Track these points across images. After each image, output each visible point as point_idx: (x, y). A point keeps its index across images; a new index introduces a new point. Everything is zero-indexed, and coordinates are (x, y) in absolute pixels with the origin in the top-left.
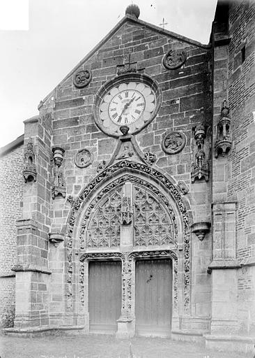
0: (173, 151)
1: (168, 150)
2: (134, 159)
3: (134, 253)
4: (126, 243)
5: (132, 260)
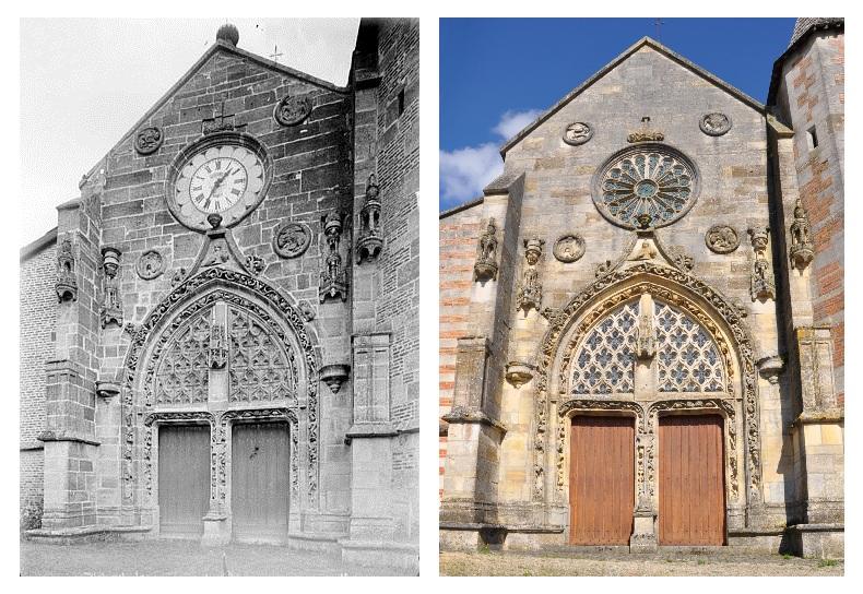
0: (723, 249)
1: (717, 245)
2: (660, 262)
3: (658, 403)
4: (647, 385)
5: (655, 414)
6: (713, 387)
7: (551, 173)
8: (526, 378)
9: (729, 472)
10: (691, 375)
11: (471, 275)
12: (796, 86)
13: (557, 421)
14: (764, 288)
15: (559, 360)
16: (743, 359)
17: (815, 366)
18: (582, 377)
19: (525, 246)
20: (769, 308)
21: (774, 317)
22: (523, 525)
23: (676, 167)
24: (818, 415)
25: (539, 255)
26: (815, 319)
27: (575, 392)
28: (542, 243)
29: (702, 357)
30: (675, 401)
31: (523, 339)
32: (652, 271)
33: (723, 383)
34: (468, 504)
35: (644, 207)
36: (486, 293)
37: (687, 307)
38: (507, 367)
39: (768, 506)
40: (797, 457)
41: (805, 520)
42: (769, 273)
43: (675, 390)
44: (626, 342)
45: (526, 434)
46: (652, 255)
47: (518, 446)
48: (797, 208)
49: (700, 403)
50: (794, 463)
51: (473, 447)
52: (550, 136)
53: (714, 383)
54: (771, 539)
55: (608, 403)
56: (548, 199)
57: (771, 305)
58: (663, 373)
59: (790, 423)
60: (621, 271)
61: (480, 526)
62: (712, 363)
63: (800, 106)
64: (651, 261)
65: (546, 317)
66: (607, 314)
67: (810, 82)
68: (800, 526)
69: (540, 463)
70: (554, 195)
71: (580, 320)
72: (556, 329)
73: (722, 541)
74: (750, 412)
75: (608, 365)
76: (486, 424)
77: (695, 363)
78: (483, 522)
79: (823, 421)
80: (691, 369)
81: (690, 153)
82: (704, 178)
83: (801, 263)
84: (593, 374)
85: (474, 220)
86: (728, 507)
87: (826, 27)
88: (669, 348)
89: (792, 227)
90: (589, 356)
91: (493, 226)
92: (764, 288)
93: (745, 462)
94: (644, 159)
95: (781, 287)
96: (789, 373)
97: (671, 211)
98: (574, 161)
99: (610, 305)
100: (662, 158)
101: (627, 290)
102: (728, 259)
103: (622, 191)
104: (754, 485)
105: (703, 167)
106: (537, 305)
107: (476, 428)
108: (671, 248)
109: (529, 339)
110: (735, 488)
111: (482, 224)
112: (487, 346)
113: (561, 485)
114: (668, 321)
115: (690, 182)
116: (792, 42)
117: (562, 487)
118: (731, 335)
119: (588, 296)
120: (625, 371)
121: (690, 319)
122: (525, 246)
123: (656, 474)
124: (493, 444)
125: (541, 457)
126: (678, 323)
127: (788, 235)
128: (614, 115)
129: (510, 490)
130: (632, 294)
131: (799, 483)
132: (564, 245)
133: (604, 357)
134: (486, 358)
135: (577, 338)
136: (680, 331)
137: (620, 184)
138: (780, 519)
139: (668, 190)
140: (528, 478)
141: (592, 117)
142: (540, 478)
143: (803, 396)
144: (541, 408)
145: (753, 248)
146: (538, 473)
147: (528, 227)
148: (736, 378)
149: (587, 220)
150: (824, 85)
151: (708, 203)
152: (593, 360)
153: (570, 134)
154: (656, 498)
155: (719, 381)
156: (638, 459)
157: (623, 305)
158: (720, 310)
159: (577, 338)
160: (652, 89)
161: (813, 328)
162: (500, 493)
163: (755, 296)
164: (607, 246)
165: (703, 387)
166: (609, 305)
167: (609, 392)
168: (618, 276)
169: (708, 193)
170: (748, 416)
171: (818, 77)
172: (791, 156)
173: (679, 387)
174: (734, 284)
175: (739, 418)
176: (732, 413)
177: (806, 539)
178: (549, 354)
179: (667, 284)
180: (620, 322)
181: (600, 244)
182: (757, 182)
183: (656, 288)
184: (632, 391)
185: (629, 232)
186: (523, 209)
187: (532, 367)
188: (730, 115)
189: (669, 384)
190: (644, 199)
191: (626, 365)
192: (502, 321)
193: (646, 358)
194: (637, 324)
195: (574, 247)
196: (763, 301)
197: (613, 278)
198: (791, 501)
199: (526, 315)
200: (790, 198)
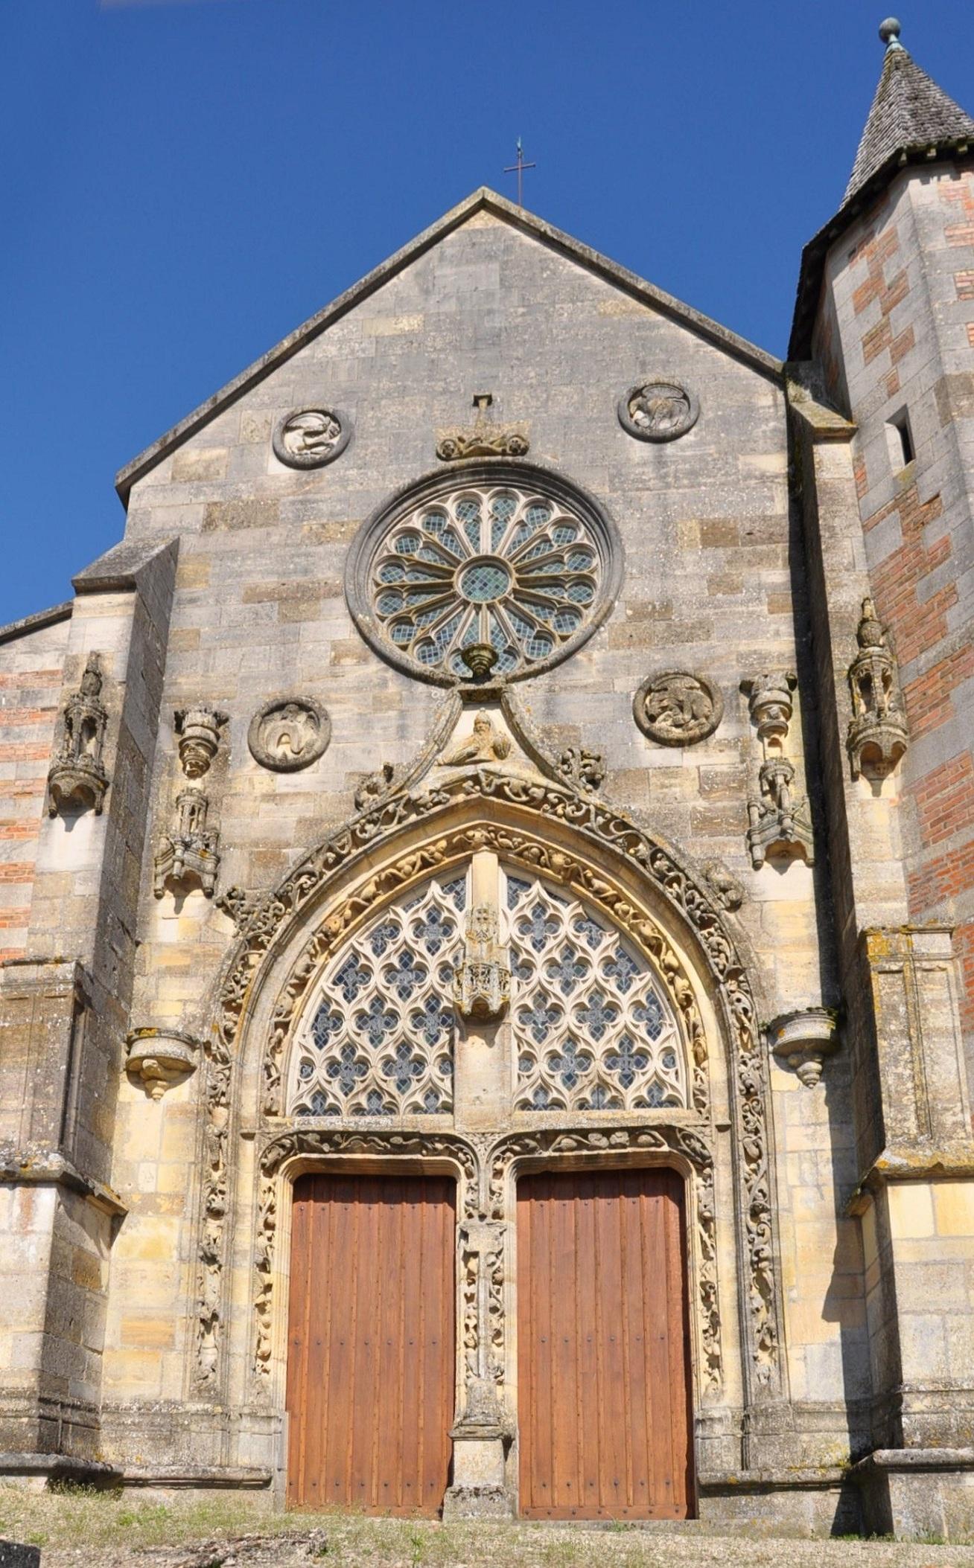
0: (677, 733)
1: (663, 724)
2: (518, 769)
3: (517, 1138)
4: (486, 1090)
5: (507, 1168)
6: (657, 1096)
7: (245, 538)
8: (177, 1071)
9: (700, 1321)
10: (598, 1065)
11: (39, 804)
12: (859, 309)
13: (256, 1185)
14: (783, 832)
15: (262, 1024)
16: (732, 1019)
17: (915, 1032)
18: (320, 1073)
19: (179, 729)
20: (797, 884)
21: (810, 908)
22: (165, 1463)
23: (560, 523)
24: (923, 1157)
25: (213, 750)
26: (913, 912)
27: (303, 1110)
28: (221, 720)
29: (626, 1017)
30: (557, 1133)
31: (170, 971)
32: (499, 792)
33: (680, 1085)
34: (23, 1404)
35: (479, 626)
36: (77, 847)
37: (589, 884)
38: (130, 1043)
39: (799, 1410)
40: (874, 1275)
41: (896, 1440)
42: (796, 794)
43: (558, 1104)
44: (433, 977)
45: (176, 1221)
46: (500, 752)
47: (152, 1252)
48: (864, 621)
49: (621, 1138)
50: (865, 1292)
51: (37, 1249)
52: (240, 448)
53: (659, 1085)
54: (810, 1498)
55: (385, 1136)
56: (234, 605)
57: (801, 877)
58: (528, 1059)
59: (852, 1187)
60: (420, 791)
61: (52, 1460)
62: (654, 1032)
63: (869, 358)
64: (496, 766)
65: (229, 912)
66: (384, 907)
67: (893, 296)
68: (884, 1455)
69: (211, 1298)
70: (254, 596)
71: (313, 923)
72: (255, 943)
73: (684, 1510)
74: (750, 1159)
75: (388, 1039)
76: (73, 1188)
77: (610, 1032)
78: (59, 1452)
79: (936, 1174)
80: (598, 1049)
81: (596, 486)
82: (630, 550)
83: (876, 763)
84: (349, 1065)
85: (50, 662)
86: (697, 1415)
87: (933, 153)
88: (543, 995)
89: (853, 669)
90: (338, 1018)
91: (95, 677)
92: (783, 832)
93: (739, 1293)
94: (476, 502)
95: (827, 830)
96: (847, 1053)
97: (545, 637)
98: (304, 506)
99: (392, 881)
100: (523, 500)
101: (434, 841)
102: (691, 759)
103: (425, 587)
104: (763, 1356)
105: (628, 524)
106: (208, 880)
107: (47, 1198)
108: (547, 733)
109: (185, 972)
110: (715, 1361)
111: (72, 662)
112: (78, 985)
113: (265, 1357)
114: (538, 923)
115: (596, 561)
116: (850, 192)
117: (268, 1365)
118: (701, 957)
119: (339, 856)
120: (432, 1054)
121: (597, 916)
122: (179, 729)
123: (511, 1325)
124: (90, 1245)
125: (213, 1282)
126: (567, 928)
127: (841, 693)
128: (404, 391)
129: (133, 1371)
130: (447, 852)
131: (878, 1345)
132: (277, 724)
133: (377, 1017)
134: (75, 1016)
135: (308, 969)
136: (570, 949)
137: (418, 567)
138: (833, 1445)
139: (540, 583)
140: (180, 1337)
141: (348, 394)
142: (210, 1339)
143: (885, 1107)
144: (213, 1151)
145: (754, 730)
146: (207, 1324)
147: (187, 680)
148: (716, 1069)
149: (336, 661)
150: (928, 302)
151: (641, 613)
152: (349, 1025)
153: (293, 441)
154: (510, 1391)
155: (670, 1079)
156: (463, 1288)
157: (426, 881)
158: (671, 892)
159: (308, 969)
160: (498, 322)
161: (908, 931)
162: (107, 1380)
163: (759, 853)
164: (384, 729)
165: (630, 1095)
166: (390, 881)
167: (391, 1109)
168: (413, 805)
169: (639, 589)
170: (745, 1168)
171: (913, 280)
172: (849, 489)
173: (568, 1096)
174: (706, 823)
175: (722, 1176)
176: (704, 1163)
177: (900, 1492)
178: (237, 1010)
179: (536, 825)
180: (419, 927)
181: (365, 723)
182: (761, 559)
183: (509, 835)
184: (449, 1108)
185: (439, 692)
186: (173, 628)
187: (192, 1043)
188: (694, 388)
189: (544, 1089)
190: (478, 607)
191: (433, 1039)
192: (118, 923)
193: (483, 1019)
194: (459, 931)
195: (303, 731)
196: (782, 868)
197: (401, 811)
198: (859, 1396)
199: (178, 909)
200: (846, 594)
